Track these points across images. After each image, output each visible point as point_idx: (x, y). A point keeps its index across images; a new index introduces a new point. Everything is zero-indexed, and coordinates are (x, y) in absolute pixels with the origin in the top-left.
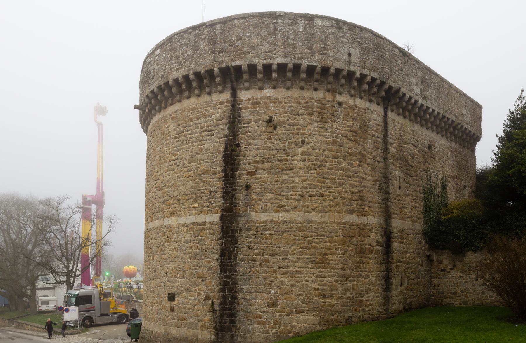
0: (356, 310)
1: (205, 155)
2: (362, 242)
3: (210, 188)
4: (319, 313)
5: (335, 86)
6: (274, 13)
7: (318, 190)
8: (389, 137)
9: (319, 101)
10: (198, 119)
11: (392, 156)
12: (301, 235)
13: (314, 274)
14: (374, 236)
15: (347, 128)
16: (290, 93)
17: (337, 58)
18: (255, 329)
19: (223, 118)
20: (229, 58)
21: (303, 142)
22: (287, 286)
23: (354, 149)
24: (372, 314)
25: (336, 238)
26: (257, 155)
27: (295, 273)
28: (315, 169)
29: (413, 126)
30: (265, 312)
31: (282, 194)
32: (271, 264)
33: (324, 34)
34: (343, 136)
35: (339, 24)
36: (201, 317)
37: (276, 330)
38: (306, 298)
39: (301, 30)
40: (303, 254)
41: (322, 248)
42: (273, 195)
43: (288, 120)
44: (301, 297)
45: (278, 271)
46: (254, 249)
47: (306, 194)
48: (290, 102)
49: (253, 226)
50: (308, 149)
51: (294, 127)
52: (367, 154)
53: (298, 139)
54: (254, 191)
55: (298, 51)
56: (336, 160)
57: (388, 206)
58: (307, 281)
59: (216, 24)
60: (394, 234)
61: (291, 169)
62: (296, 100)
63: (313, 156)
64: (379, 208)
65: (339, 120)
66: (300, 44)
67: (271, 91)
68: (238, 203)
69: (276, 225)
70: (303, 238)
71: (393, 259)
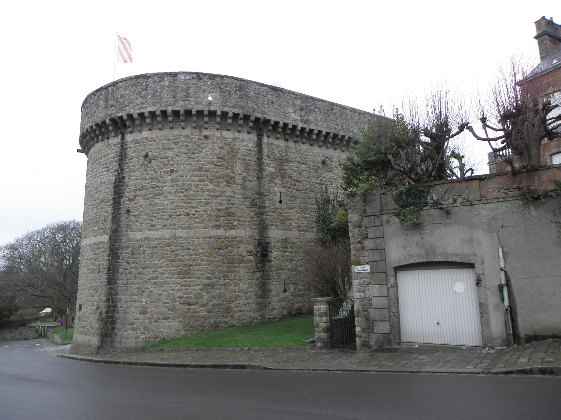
0: (223, 316)
2: (230, 253)
3: (105, 213)
4: (184, 319)
5: (200, 123)
6: (146, 75)
7: (185, 210)
8: (264, 159)
10: (101, 159)
11: (270, 175)
14: (245, 247)
15: (213, 156)
16: (162, 133)
18: (128, 335)
19: (115, 157)
20: (115, 111)
21: (172, 171)
22: (156, 295)
23: (220, 173)
24: (243, 320)
25: (202, 251)
27: (163, 283)
28: (182, 193)
29: (300, 146)
30: (137, 319)
32: (143, 276)
33: (186, 86)
34: (209, 163)
35: (199, 76)
37: (146, 336)
38: (172, 305)
39: (167, 84)
40: (170, 267)
41: (187, 260)
42: (147, 216)
43: (160, 154)
44: (167, 305)
45: (149, 282)
47: (174, 214)
48: (162, 140)
49: (131, 244)
51: (165, 159)
52: (236, 176)
53: (168, 169)
54: (133, 214)
55: (164, 101)
56: (202, 183)
57: (263, 219)
58: (173, 290)
59: (109, 86)
60: (272, 244)
61: (162, 194)
62: (167, 138)
63: (181, 182)
65: (205, 150)
67: (148, 132)
68: (121, 225)
69: (148, 242)
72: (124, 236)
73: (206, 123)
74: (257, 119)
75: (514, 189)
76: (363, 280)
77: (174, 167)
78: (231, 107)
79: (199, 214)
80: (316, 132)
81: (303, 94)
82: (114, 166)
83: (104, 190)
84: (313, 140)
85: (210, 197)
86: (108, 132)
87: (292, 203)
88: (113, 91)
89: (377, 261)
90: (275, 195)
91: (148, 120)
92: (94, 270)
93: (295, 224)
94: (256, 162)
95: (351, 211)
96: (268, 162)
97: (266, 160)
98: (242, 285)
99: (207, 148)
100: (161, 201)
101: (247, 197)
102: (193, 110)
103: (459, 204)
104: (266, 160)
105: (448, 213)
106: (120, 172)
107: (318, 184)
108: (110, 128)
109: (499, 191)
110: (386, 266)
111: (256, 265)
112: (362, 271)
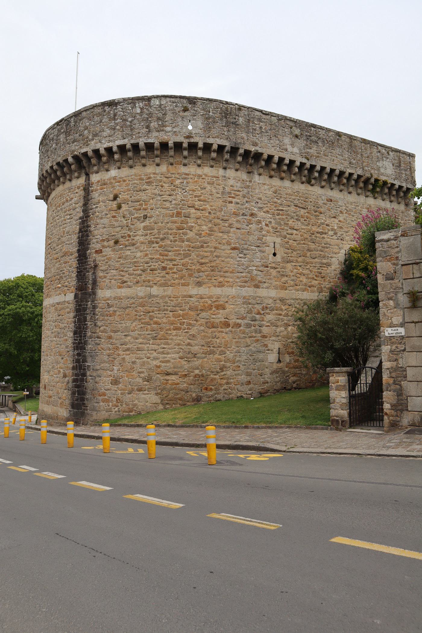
7: (161, 263)
13: (155, 351)
16: (133, 171)
25: (182, 312)
27: (137, 349)
30: (108, 390)
31: (125, 269)
36: (60, 395)
37: (119, 409)
40: (144, 330)
44: (142, 375)
53: (140, 214)
54: (101, 268)
56: (181, 231)
58: (148, 358)
62: (139, 177)
65: (184, 191)
67: (117, 171)
69: (119, 302)
70: (144, 313)
83: (68, 241)
86: (71, 172)
91: (116, 156)
93: (291, 282)
102: (169, 142)
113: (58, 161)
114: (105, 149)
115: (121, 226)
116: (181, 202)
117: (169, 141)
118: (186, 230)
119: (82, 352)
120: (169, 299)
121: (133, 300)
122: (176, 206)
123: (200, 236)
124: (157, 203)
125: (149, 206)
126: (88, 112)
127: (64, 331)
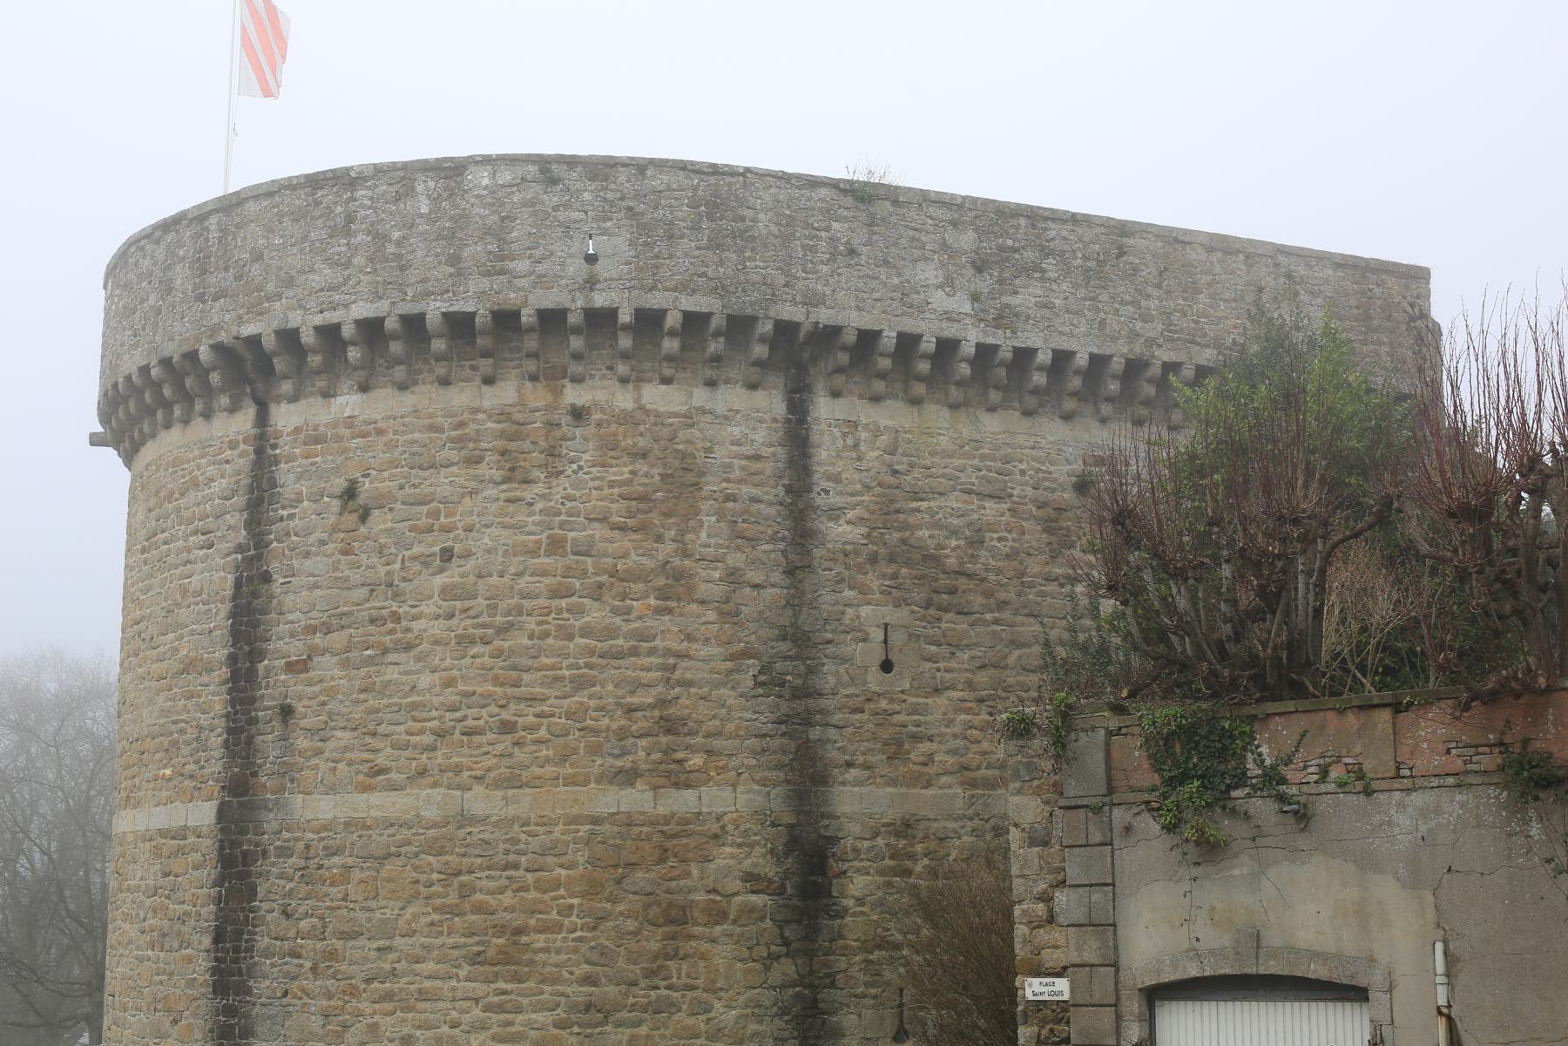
1: (192, 608)
2: (674, 884)
3: (199, 715)
7: (497, 710)
8: (817, 489)
9: (503, 415)
10: (182, 495)
12: (435, 865)
13: (477, 1001)
14: (732, 856)
15: (606, 491)
16: (409, 400)
17: (540, 276)
20: (234, 313)
21: (447, 555)
25: (564, 872)
26: (313, 607)
27: (416, 996)
31: (381, 729)
32: (344, 967)
35: (549, 170)
39: (424, 210)
40: (441, 933)
41: (506, 909)
42: (356, 734)
43: (401, 487)
46: (297, 916)
50: (462, 576)
51: (419, 508)
54: (303, 723)
55: (413, 276)
56: (564, 603)
57: (808, 740)
59: (210, 213)
60: (850, 842)
61: (409, 647)
62: (427, 422)
63: (480, 599)
64: (755, 753)
65: (575, 466)
66: (420, 254)
67: (356, 398)
69: (360, 836)
70: (442, 877)
71: (841, 936)
72: (270, 810)
73: (577, 357)
74: (786, 330)
75: (1490, 746)
76: (1048, 1027)
77: (455, 539)
78: (675, 289)
79: (549, 726)
80: (1044, 357)
81: (986, 202)
82: (230, 528)
83: (197, 622)
84: (1035, 392)
85: (594, 660)
86: (208, 391)
87: (938, 670)
88: (224, 231)
89: (1092, 966)
90: (864, 640)
91: (353, 354)
92: (165, 935)
93: (947, 758)
94: (781, 504)
95: (1017, 785)
96: (835, 500)
97: (827, 492)
98: (721, 1010)
99: (580, 459)
100: (407, 673)
101: (744, 654)
102: (523, 312)
103: (1334, 785)
104: (827, 492)
105: (1302, 817)
106: (252, 552)
107: (1056, 579)
108: (215, 378)
109: (1448, 752)
110: (1117, 983)
111: (781, 928)
112: (1046, 998)
113: (167, 353)
114: (318, 329)
115: (370, 584)
116: (562, 503)
117: (520, 307)
118: (580, 597)
119: (239, 1002)
120: (524, 829)
121: (406, 833)
122: (546, 519)
123: (626, 617)
124: (487, 508)
125: (458, 517)
126: (265, 203)
127: (183, 928)
